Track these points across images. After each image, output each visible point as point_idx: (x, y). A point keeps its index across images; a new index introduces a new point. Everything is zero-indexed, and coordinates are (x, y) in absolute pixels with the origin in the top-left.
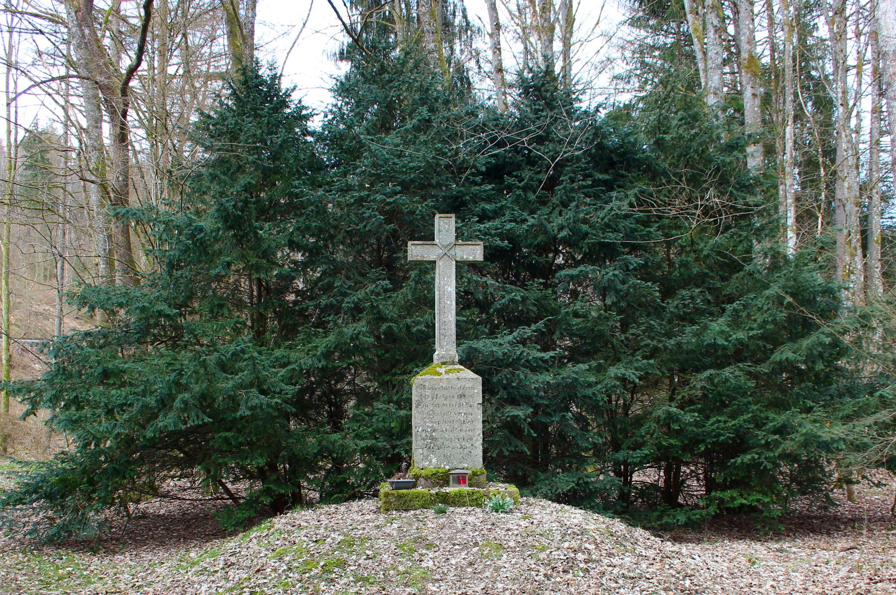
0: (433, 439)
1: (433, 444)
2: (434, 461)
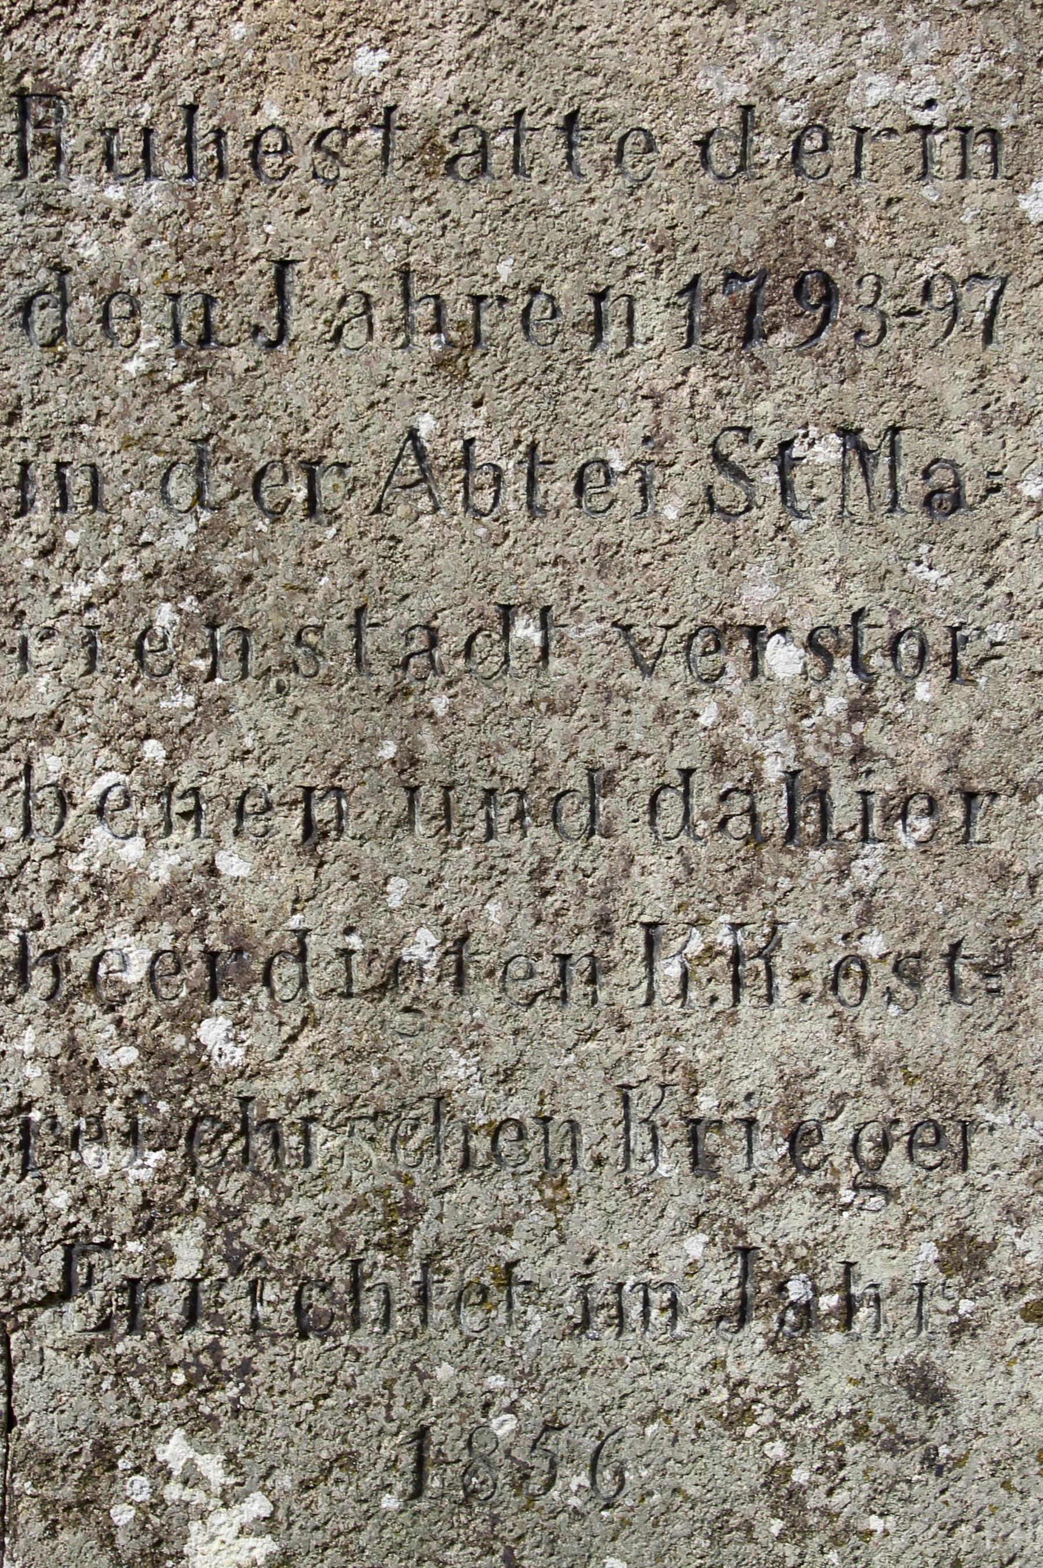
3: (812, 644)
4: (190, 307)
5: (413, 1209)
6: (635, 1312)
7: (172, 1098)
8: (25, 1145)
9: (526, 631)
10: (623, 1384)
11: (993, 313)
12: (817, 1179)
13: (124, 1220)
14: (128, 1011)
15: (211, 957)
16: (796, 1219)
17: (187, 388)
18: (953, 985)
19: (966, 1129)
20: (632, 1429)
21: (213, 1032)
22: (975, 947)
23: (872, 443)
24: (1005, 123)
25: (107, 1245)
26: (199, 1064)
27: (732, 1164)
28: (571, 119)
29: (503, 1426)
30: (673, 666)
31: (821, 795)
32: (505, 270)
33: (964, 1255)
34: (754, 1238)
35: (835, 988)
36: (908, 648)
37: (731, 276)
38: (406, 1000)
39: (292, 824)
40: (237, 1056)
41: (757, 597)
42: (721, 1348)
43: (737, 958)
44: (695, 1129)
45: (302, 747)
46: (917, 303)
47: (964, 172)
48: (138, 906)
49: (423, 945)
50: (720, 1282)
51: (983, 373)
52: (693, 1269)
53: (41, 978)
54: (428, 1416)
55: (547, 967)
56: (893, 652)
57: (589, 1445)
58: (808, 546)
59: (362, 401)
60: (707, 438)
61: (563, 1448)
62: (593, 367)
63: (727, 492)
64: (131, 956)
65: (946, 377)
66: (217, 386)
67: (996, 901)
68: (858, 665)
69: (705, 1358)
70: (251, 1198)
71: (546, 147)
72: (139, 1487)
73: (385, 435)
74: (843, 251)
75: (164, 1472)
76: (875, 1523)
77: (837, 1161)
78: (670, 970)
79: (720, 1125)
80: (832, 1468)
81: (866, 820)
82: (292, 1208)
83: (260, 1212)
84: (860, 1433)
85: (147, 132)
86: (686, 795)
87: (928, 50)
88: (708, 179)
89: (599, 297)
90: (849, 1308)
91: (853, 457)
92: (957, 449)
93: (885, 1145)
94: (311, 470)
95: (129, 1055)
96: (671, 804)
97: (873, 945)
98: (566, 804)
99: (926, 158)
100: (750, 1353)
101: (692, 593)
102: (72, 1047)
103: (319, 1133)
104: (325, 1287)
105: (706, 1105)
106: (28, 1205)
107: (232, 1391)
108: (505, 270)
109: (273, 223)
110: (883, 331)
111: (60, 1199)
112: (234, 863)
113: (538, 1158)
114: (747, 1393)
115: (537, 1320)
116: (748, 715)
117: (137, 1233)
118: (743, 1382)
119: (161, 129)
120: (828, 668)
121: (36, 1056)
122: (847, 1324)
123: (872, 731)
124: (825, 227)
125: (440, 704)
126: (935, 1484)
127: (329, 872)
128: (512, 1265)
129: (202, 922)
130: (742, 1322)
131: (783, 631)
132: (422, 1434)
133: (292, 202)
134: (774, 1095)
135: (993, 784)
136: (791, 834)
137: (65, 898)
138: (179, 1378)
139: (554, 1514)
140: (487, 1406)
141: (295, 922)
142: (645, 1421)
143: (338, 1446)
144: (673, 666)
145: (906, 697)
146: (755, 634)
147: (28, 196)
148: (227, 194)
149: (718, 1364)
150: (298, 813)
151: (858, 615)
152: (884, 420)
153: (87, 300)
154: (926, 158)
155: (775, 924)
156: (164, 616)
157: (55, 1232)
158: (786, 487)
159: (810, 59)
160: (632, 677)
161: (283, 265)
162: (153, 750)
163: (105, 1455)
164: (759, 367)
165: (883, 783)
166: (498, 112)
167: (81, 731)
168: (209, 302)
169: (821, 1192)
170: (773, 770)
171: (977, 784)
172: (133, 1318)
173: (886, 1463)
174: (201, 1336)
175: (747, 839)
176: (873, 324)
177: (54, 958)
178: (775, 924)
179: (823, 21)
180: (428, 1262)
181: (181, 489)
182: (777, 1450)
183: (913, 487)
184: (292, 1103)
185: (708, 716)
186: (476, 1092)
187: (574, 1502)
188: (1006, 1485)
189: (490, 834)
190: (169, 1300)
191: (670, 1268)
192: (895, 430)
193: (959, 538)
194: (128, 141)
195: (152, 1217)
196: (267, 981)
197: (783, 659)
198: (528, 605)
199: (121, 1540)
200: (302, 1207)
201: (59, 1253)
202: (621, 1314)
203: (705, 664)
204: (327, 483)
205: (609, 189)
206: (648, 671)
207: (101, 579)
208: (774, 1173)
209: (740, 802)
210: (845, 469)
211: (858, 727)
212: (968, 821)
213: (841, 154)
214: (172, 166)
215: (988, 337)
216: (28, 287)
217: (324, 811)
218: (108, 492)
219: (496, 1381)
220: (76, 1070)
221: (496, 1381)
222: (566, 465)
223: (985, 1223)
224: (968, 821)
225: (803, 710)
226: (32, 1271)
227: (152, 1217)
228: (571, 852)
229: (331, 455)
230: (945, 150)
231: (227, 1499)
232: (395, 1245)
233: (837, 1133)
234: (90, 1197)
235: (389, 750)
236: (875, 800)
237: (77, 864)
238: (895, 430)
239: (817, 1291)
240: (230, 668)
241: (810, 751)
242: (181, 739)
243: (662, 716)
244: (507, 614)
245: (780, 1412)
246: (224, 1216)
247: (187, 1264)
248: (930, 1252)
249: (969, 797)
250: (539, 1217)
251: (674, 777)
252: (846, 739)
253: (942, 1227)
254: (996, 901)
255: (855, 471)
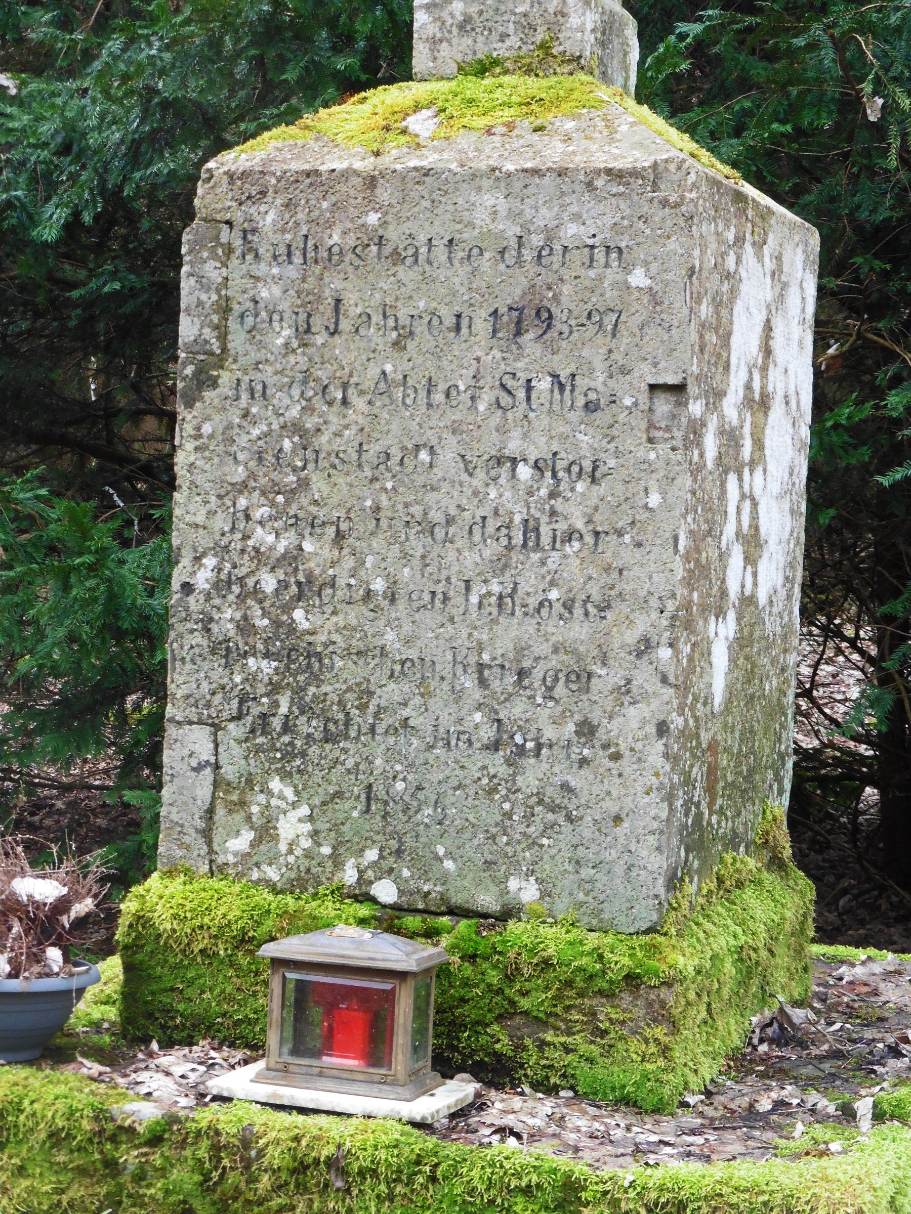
0: (300, 658)
1: (302, 715)
2: (292, 827)
3: (536, 466)
4: (303, 317)
5: (371, 694)
6: (453, 743)
7: (282, 641)
8: (226, 656)
9: (424, 456)
10: (447, 772)
11: (616, 325)
12: (528, 692)
13: (261, 689)
14: (267, 604)
15: (299, 584)
16: (518, 709)
17: (299, 351)
18: (586, 614)
19: (590, 675)
20: (450, 792)
21: (298, 614)
22: (596, 597)
23: (563, 380)
24: (623, 245)
25: (255, 699)
26: (292, 629)
27: (495, 685)
28: (451, 241)
29: (400, 786)
30: (481, 474)
31: (537, 530)
32: (422, 304)
33: (586, 730)
34: (501, 716)
35: (539, 612)
36: (575, 469)
37: (511, 309)
38: (371, 606)
39: (331, 531)
40: (306, 625)
41: (513, 447)
42: (486, 762)
43: (501, 597)
44: (481, 667)
45: (336, 499)
46: (584, 321)
47: (607, 265)
48: (272, 561)
49: (378, 585)
50: (487, 733)
51: (610, 351)
52: (476, 727)
53: (236, 589)
54: (372, 779)
55: (427, 597)
56: (568, 470)
57: (433, 798)
58: (536, 424)
59: (364, 357)
60: (497, 377)
61: (422, 798)
62: (455, 347)
63: (505, 400)
64: (269, 583)
65: (594, 354)
66: (310, 351)
67: (605, 579)
68: (554, 475)
69: (480, 764)
70: (309, 684)
71: (440, 253)
72: (261, 798)
73: (373, 372)
74: (556, 298)
75: (270, 793)
76: (545, 841)
77: (536, 685)
78: (474, 599)
79: (490, 667)
80: (529, 817)
81: (554, 542)
82: (326, 688)
83: (312, 690)
84: (540, 802)
85: (289, 246)
86: (484, 526)
87: (593, 213)
88: (502, 267)
89: (459, 316)
90: (539, 747)
91: (556, 386)
92: (598, 384)
93: (556, 679)
94: (345, 386)
95: (266, 622)
96: (477, 530)
97: (554, 595)
98: (437, 529)
99: (592, 260)
100: (497, 763)
101: (489, 444)
102: (245, 618)
103: (336, 659)
104: (336, 722)
105: (486, 657)
106: (225, 681)
107: (298, 762)
108: (422, 304)
109: (334, 283)
110: (571, 333)
111: (238, 679)
112: (308, 546)
113: (419, 675)
114: (496, 781)
115: (415, 742)
116: (508, 494)
117: (267, 695)
118: (494, 776)
119: (294, 245)
120: (543, 476)
121: (231, 620)
122: (538, 755)
123: (558, 504)
124: (550, 288)
125: (389, 485)
126: (570, 827)
127: (345, 551)
128: (407, 719)
129: (296, 570)
130: (497, 750)
131: (524, 460)
132: (370, 786)
133: (342, 276)
134: (511, 655)
135: (606, 528)
136: (525, 545)
137: (246, 557)
138: (278, 755)
139: (418, 825)
140: (395, 777)
141: (331, 572)
142: (455, 789)
143: (337, 788)
144: (481, 474)
145: (572, 489)
146: (514, 461)
147: (244, 272)
148: (317, 272)
149: (485, 767)
150: (334, 528)
151: (555, 454)
152: (568, 371)
153: (264, 314)
154: (592, 260)
155: (516, 584)
156: (287, 444)
157: (236, 692)
158: (528, 399)
159: (545, 216)
160: (465, 477)
161: (338, 301)
162: (280, 499)
163: (250, 782)
164: (520, 347)
165: (562, 526)
166: (422, 238)
167: (254, 489)
168: (309, 315)
169: (529, 698)
170: (517, 519)
171: (599, 529)
172: (263, 729)
173: (550, 816)
174: (286, 739)
175: (506, 547)
176: (566, 329)
177: (241, 580)
178: (516, 584)
179: (551, 200)
180: (376, 715)
181: (296, 392)
182: (507, 806)
183: (580, 402)
184: (326, 646)
185: (493, 494)
186: (397, 645)
187: (426, 820)
188: (599, 830)
189: (407, 539)
190: (276, 723)
191: (468, 725)
192: (573, 376)
193: (597, 423)
194: (282, 250)
195: (275, 688)
196: (320, 596)
197: (524, 472)
198: (425, 445)
199: (254, 819)
200: (326, 688)
201: (236, 700)
202: (449, 743)
203: (493, 473)
204: (351, 391)
205: (463, 271)
206: (471, 475)
207: (265, 428)
208: (510, 689)
209: (504, 531)
210: (552, 391)
211: (553, 502)
212: (596, 544)
213: (557, 258)
214: (297, 259)
215: (614, 335)
216: (242, 309)
217: (344, 526)
218: (268, 392)
219: (398, 767)
220: (245, 626)
221: (398, 767)
222: (442, 387)
223: (595, 717)
224: (596, 544)
225: (530, 494)
226: (227, 707)
227: (275, 688)
228: (437, 549)
229: (352, 381)
230: (599, 254)
231: (294, 805)
232: (363, 707)
233: (538, 674)
234: (251, 679)
235: (369, 503)
236: (558, 533)
237: (250, 543)
238: (573, 376)
239: (525, 740)
240: (311, 466)
241: (532, 511)
242: (291, 494)
243: (476, 493)
244: (417, 447)
245: (509, 790)
246: (299, 691)
247: (283, 710)
248: (571, 727)
249: (597, 534)
250: (418, 700)
251: (478, 519)
252: (547, 507)
253: (577, 717)
254: (605, 579)
255: (556, 391)
